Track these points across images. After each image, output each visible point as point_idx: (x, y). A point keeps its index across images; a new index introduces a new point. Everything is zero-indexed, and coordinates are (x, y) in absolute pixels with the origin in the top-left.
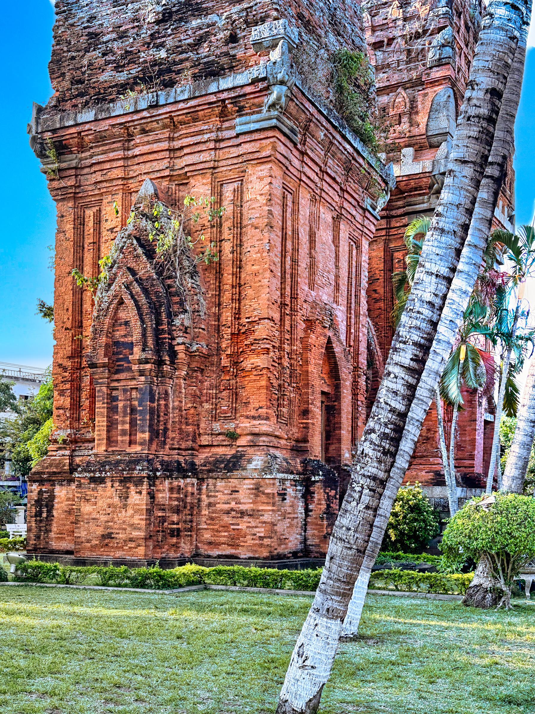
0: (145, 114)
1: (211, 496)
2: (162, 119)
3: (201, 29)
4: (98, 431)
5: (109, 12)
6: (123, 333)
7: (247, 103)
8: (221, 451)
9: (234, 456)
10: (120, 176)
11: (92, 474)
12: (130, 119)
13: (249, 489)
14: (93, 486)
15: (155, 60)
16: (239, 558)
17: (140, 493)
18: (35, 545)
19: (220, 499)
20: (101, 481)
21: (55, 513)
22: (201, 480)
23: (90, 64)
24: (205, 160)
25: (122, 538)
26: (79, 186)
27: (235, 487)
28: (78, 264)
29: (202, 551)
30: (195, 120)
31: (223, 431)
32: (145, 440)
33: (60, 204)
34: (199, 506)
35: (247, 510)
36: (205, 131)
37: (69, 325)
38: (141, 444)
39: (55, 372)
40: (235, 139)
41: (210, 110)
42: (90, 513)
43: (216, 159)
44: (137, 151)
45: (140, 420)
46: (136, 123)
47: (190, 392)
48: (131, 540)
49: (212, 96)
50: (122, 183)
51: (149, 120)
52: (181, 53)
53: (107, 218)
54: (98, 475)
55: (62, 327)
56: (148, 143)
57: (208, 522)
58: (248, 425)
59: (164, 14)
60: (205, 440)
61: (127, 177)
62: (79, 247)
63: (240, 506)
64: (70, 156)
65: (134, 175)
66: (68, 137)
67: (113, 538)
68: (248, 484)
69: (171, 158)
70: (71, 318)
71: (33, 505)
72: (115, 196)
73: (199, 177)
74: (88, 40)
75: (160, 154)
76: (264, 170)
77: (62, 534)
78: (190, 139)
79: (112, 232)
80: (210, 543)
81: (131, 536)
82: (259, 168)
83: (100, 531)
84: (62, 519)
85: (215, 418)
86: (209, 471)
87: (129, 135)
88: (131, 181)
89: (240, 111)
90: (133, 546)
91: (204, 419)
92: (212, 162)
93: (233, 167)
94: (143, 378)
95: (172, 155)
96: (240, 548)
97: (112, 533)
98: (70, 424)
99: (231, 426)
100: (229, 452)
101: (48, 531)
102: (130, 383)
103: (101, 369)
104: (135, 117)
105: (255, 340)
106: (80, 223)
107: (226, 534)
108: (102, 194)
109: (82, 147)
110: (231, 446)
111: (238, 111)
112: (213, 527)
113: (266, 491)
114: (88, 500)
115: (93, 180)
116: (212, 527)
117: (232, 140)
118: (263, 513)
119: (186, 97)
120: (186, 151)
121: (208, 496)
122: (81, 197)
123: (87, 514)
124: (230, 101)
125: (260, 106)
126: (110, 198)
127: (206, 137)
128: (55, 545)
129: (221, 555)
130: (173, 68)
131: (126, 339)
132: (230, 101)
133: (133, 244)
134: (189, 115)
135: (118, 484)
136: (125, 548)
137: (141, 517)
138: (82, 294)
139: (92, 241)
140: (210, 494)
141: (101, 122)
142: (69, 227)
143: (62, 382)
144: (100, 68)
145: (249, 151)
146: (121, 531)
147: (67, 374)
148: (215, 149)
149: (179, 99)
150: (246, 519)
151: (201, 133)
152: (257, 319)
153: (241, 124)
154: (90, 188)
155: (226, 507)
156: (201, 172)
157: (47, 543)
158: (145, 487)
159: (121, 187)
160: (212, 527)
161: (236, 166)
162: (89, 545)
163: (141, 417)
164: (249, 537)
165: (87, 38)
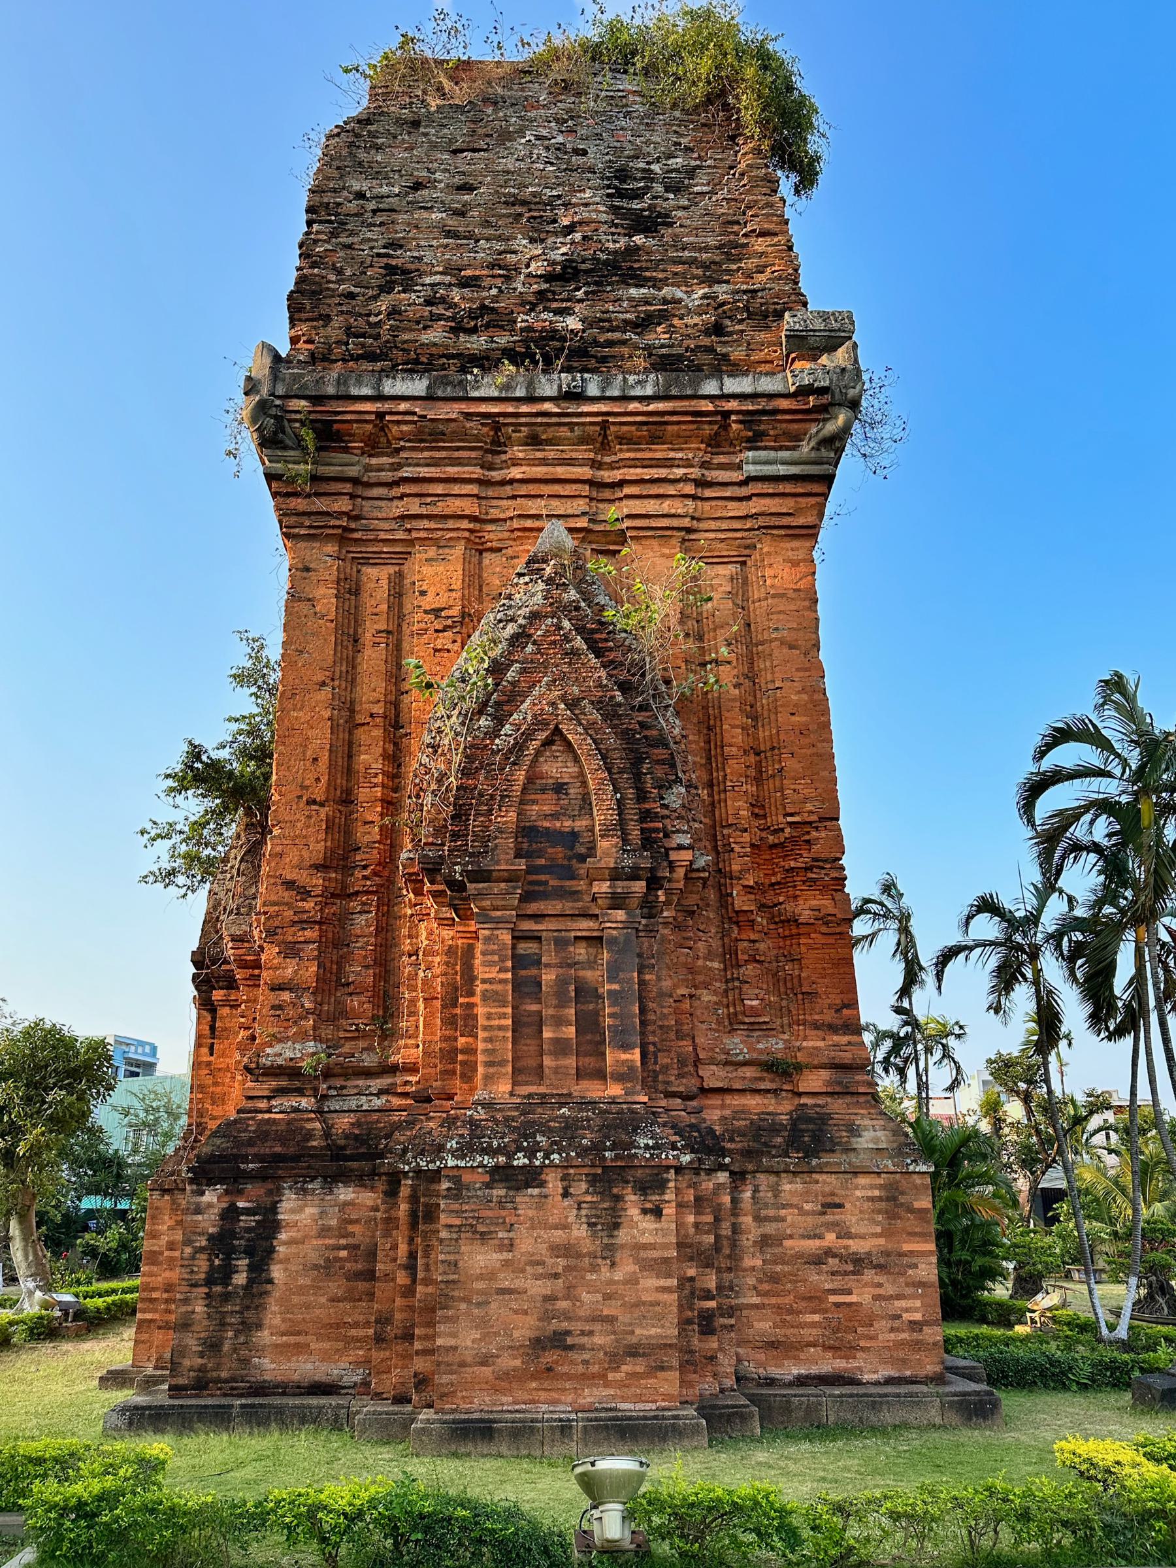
0: (548, 406)
1: (767, 1219)
2: (583, 424)
3: (647, 303)
4: (485, 1040)
5: (434, 243)
6: (547, 809)
7: (774, 428)
8: (753, 1102)
9: (800, 1118)
10: (467, 512)
11: (502, 1159)
12: (511, 410)
13: (872, 1199)
14: (502, 1192)
15: (555, 331)
16: (858, 1383)
17: (657, 1212)
18: (202, 1369)
19: (792, 1225)
20: (532, 1177)
21: (277, 1272)
22: (739, 1177)
23: (394, 312)
24: (673, 511)
25: (601, 1347)
26: (357, 518)
27: (833, 1194)
28: (344, 668)
29: (751, 1369)
30: (655, 439)
31: (755, 1055)
32: (632, 1068)
33: (302, 545)
34: (734, 1244)
35: (869, 1254)
36: (676, 463)
37: (319, 793)
38: (619, 1078)
39: (274, 898)
40: (736, 488)
41: (695, 426)
42: (491, 1276)
43: (696, 515)
44: (516, 473)
45: (611, 1015)
46: (523, 420)
47: (682, 959)
48: (633, 1352)
49: (703, 402)
50: (471, 526)
51: (554, 420)
52: (612, 330)
53: (424, 588)
54: (521, 1160)
55: (300, 797)
56: (544, 462)
57: (765, 1287)
58: (821, 1044)
59: (564, 268)
60: (713, 1076)
61: (483, 517)
62: (350, 639)
63: (850, 1242)
64: (346, 457)
65: (502, 516)
66: (349, 417)
67: (571, 1348)
68: (864, 1188)
69: (592, 499)
70: (324, 780)
71: (202, 1249)
72: (447, 550)
73: (655, 543)
74: (385, 275)
75: (568, 487)
76: (797, 549)
77: (298, 1333)
78: (639, 470)
79: (437, 617)
80: (773, 1345)
81: (634, 1340)
82: (788, 545)
83: (524, 1329)
84: (301, 1290)
85: (733, 1023)
86: (748, 1154)
87: (496, 442)
88: (490, 527)
89: (754, 442)
90: (640, 1369)
91: (704, 1026)
92: (688, 519)
93: (730, 535)
94: (620, 915)
95: (594, 494)
96: (858, 1355)
97: (568, 1333)
98: (315, 1028)
99: (775, 1045)
100: (782, 1108)
101: (249, 1327)
102: (571, 925)
103: (503, 885)
104: (524, 409)
105: (815, 860)
106: (350, 590)
107: (817, 1318)
108: (411, 542)
109: (372, 446)
110: (775, 1092)
111: (749, 440)
112: (780, 1300)
113: (917, 1205)
114: (484, 1237)
115: (398, 512)
116: (773, 1300)
117: (730, 488)
118: (915, 1260)
119: (649, 391)
120: (628, 490)
121: (757, 1219)
122: (356, 540)
123: (481, 1277)
124: (741, 417)
125: (798, 438)
126: (432, 552)
127: (679, 472)
128: (269, 1368)
129: (807, 1377)
130: (592, 351)
131: (558, 824)
132: (741, 417)
133: (562, 628)
134: (645, 428)
135: (584, 1186)
136: (611, 1376)
137: (663, 1282)
138: (350, 733)
139: (384, 627)
140: (763, 1213)
141: (440, 404)
142: (326, 596)
143: (294, 923)
144: (418, 323)
145: (773, 510)
146: (597, 1327)
147: (309, 905)
148: (694, 497)
149: (633, 393)
150: (869, 1275)
151: (668, 463)
152: (814, 818)
153: (753, 462)
154: (386, 525)
155: (813, 1245)
156: (659, 533)
157: (245, 1362)
158: (669, 1196)
159: (467, 534)
160: (773, 1300)
161: (739, 535)
162: (487, 1371)
163: (616, 1009)
164: (882, 1325)
165: (382, 271)
